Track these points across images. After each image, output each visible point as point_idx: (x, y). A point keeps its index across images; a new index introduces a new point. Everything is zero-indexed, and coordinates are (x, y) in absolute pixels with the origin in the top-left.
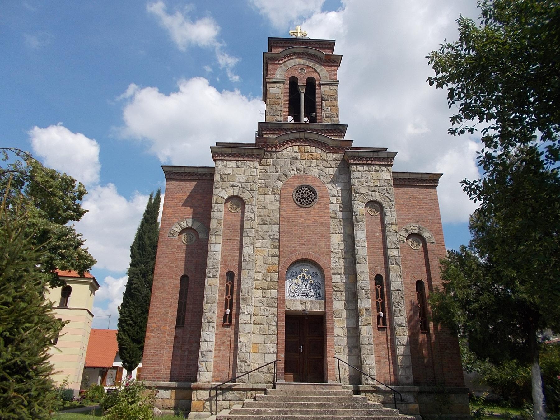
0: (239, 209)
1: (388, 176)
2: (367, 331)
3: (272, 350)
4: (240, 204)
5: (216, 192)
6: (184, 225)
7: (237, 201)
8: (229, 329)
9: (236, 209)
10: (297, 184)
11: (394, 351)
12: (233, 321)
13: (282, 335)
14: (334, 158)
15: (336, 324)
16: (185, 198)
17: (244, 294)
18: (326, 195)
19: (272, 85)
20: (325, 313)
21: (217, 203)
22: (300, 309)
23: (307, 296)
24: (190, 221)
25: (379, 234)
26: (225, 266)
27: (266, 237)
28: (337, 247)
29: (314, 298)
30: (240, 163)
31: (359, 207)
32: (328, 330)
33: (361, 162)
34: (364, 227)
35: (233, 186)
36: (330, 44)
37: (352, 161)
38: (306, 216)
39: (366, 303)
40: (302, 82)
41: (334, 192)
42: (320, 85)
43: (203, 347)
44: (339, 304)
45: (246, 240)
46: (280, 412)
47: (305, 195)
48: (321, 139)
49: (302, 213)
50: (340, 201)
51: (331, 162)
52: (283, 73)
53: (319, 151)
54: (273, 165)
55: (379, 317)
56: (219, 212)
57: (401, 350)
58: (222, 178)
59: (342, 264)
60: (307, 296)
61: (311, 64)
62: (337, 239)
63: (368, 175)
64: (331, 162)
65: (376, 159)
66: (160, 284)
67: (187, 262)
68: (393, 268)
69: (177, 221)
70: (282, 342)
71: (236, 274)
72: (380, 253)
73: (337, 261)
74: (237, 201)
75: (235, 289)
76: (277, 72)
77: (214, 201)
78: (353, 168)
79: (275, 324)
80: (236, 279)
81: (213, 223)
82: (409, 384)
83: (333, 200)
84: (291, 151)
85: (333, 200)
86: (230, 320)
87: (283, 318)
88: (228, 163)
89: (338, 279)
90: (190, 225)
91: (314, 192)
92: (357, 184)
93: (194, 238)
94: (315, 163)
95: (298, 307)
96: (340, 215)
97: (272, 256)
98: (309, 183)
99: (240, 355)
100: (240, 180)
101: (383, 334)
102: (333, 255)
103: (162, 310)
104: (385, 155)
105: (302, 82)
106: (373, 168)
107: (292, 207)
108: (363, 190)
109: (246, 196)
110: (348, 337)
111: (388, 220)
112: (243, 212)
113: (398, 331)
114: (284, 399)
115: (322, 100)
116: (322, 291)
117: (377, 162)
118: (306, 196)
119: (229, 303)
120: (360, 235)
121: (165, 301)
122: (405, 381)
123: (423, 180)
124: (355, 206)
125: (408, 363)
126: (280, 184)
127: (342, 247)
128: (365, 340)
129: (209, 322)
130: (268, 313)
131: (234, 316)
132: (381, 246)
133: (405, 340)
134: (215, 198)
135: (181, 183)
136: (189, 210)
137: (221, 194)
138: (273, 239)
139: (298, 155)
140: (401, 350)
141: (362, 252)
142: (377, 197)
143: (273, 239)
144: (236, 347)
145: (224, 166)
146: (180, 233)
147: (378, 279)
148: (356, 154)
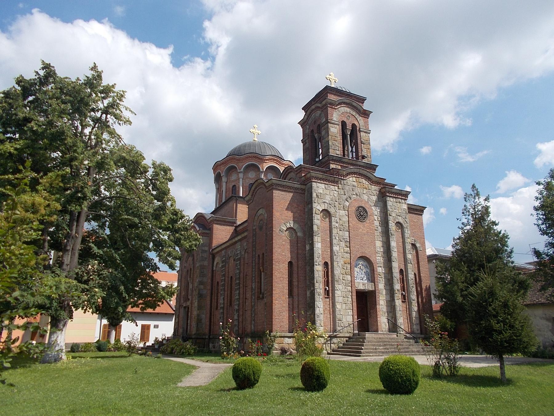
0: (327, 219)
1: (405, 207)
2: (398, 302)
3: (350, 314)
4: (328, 215)
5: (315, 205)
6: (288, 226)
7: (327, 213)
8: (328, 300)
9: (325, 219)
10: (357, 205)
11: (410, 315)
12: (330, 294)
13: (355, 304)
14: (375, 189)
15: (381, 298)
16: (287, 205)
17: (336, 278)
18: (372, 215)
19: (332, 125)
20: (375, 291)
21: (316, 213)
22: (362, 288)
23: (362, 280)
24: (292, 222)
25: (401, 244)
26: (323, 258)
27: (342, 240)
28: (379, 250)
29: (366, 281)
30: (326, 186)
31: (392, 226)
32: (377, 302)
33: (392, 195)
34: (395, 239)
35: (324, 202)
36: (362, 100)
37: (388, 194)
38: (362, 227)
39: (397, 286)
40: (349, 127)
41: (375, 212)
42: (360, 131)
43: (317, 311)
44: (381, 286)
45: (335, 241)
46: (385, 349)
47: (362, 214)
48: (365, 173)
49: (360, 225)
50: (379, 219)
51: (373, 192)
52: (338, 117)
53: (367, 183)
54: (343, 189)
55: (325, 289)
56: (318, 221)
57: (414, 314)
58: (317, 196)
59: (382, 261)
60: (362, 280)
61: (354, 113)
62: (379, 244)
63: (395, 204)
64: (373, 192)
65: (400, 194)
66: (277, 267)
67: (291, 252)
68: (410, 266)
69: (283, 221)
70: (355, 309)
71: (329, 264)
72: (402, 255)
73: (379, 260)
74: (327, 213)
75: (330, 273)
76: (334, 115)
77: (314, 212)
78: (388, 199)
79: (350, 297)
80: (330, 267)
81: (315, 228)
82: (418, 334)
83: (376, 217)
84: (351, 180)
85: (376, 217)
86: (329, 293)
87: (354, 294)
88: (320, 185)
89: (380, 270)
90: (292, 226)
91: (366, 212)
92: (390, 210)
93: (294, 235)
94: (365, 191)
95: (361, 287)
96: (380, 229)
97: (346, 253)
98: (363, 205)
99: (338, 316)
100: (328, 199)
101: (404, 305)
102: (377, 255)
103: (281, 285)
104: (405, 193)
105: (349, 127)
106: (398, 200)
107: (354, 221)
108: (394, 215)
109: (332, 210)
110: (387, 306)
111: (407, 235)
112: (330, 222)
113: (413, 304)
114: (378, 342)
115: (362, 143)
116: (372, 278)
117: (400, 197)
118: (362, 214)
119: (327, 283)
120: (393, 244)
121: (282, 279)
122: (416, 332)
123: (417, 210)
124: (390, 225)
125: (418, 322)
126: (347, 204)
127: (382, 250)
128: (398, 309)
129: (319, 295)
130: (346, 290)
131: (330, 292)
132: (402, 252)
133: (416, 309)
134: (314, 210)
135: (283, 193)
136: (290, 214)
137: (318, 208)
138: (346, 242)
139: (355, 184)
140: (414, 314)
141: (395, 255)
142: (401, 220)
143: (346, 242)
144: (334, 312)
145: (318, 187)
146: (286, 231)
147: (401, 271)
148: (390, 190)
